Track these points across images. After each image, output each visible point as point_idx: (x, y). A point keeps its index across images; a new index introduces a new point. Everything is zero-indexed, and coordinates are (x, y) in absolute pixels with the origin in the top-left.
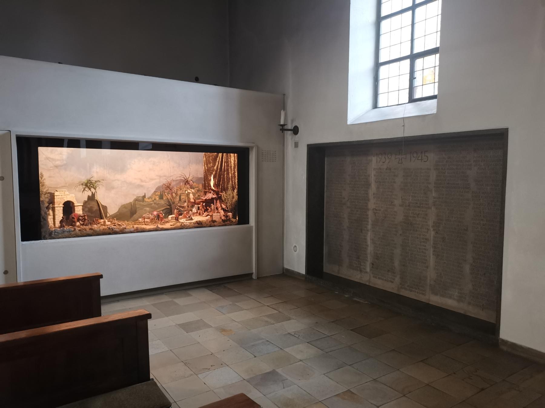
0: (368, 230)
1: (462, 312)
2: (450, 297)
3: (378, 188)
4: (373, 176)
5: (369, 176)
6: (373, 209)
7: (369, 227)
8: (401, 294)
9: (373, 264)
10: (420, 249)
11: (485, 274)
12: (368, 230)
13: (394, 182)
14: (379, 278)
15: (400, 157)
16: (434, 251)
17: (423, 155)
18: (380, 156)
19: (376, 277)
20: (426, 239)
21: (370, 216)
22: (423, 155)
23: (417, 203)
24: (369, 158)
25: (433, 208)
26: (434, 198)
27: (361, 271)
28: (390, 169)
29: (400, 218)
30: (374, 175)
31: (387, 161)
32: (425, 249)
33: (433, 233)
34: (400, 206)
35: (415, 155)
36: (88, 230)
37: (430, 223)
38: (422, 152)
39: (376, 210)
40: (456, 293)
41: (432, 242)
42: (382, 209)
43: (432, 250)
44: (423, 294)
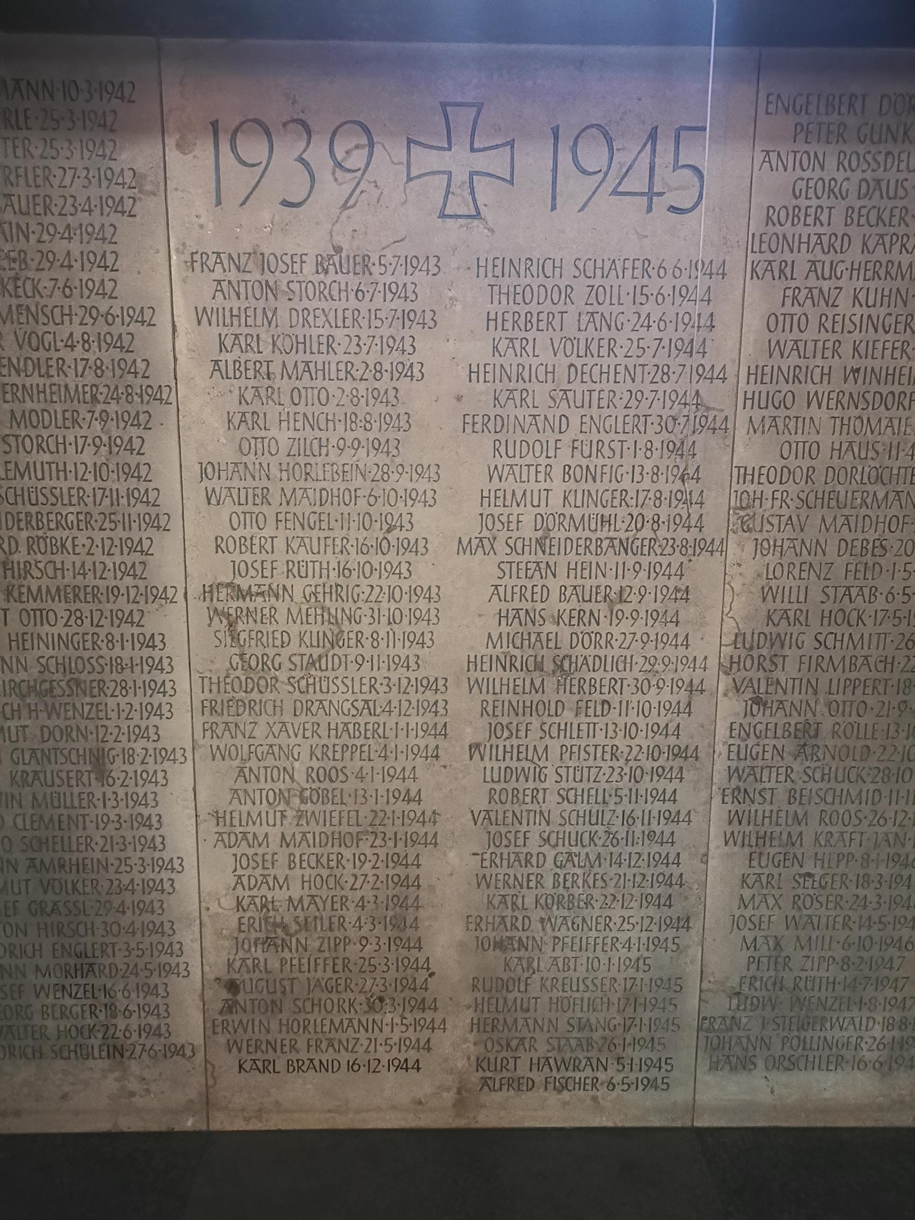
0: (167, 755)
2: (836, 1059)
3: (245, 420)
4: (184, 321)
5: (143, 317)
6: (209, 592)
7: (180, 727)
9: (232, 986)
10: (628, 819)
12: (167, 755)
13: (406, 372)
14: (295, 1067)
15: (459, 161)
16: (735, 818)
17: (665, 156)
18: (253, 148)
19: (267, 1067)
20: (679, 753)
21: (176, 647)
22: (665, 156)
23: (604, 521)
24: (137, 156)
25: (738, 549)
26: (744, 474)
27: (117, 1052)
28: (363, 264)
29: (465, 621)
30: (201, 316)
31: (331, 190)
32: (672, 818)
33: (729, 709)
34: (689, 947)
35: (594, 155)
36: (831, 162)
37: (711, 643)
38: (653, 136)
39: (241, 594)
40: (877, 1032)
42: (299, 586)
43: (718, 811)
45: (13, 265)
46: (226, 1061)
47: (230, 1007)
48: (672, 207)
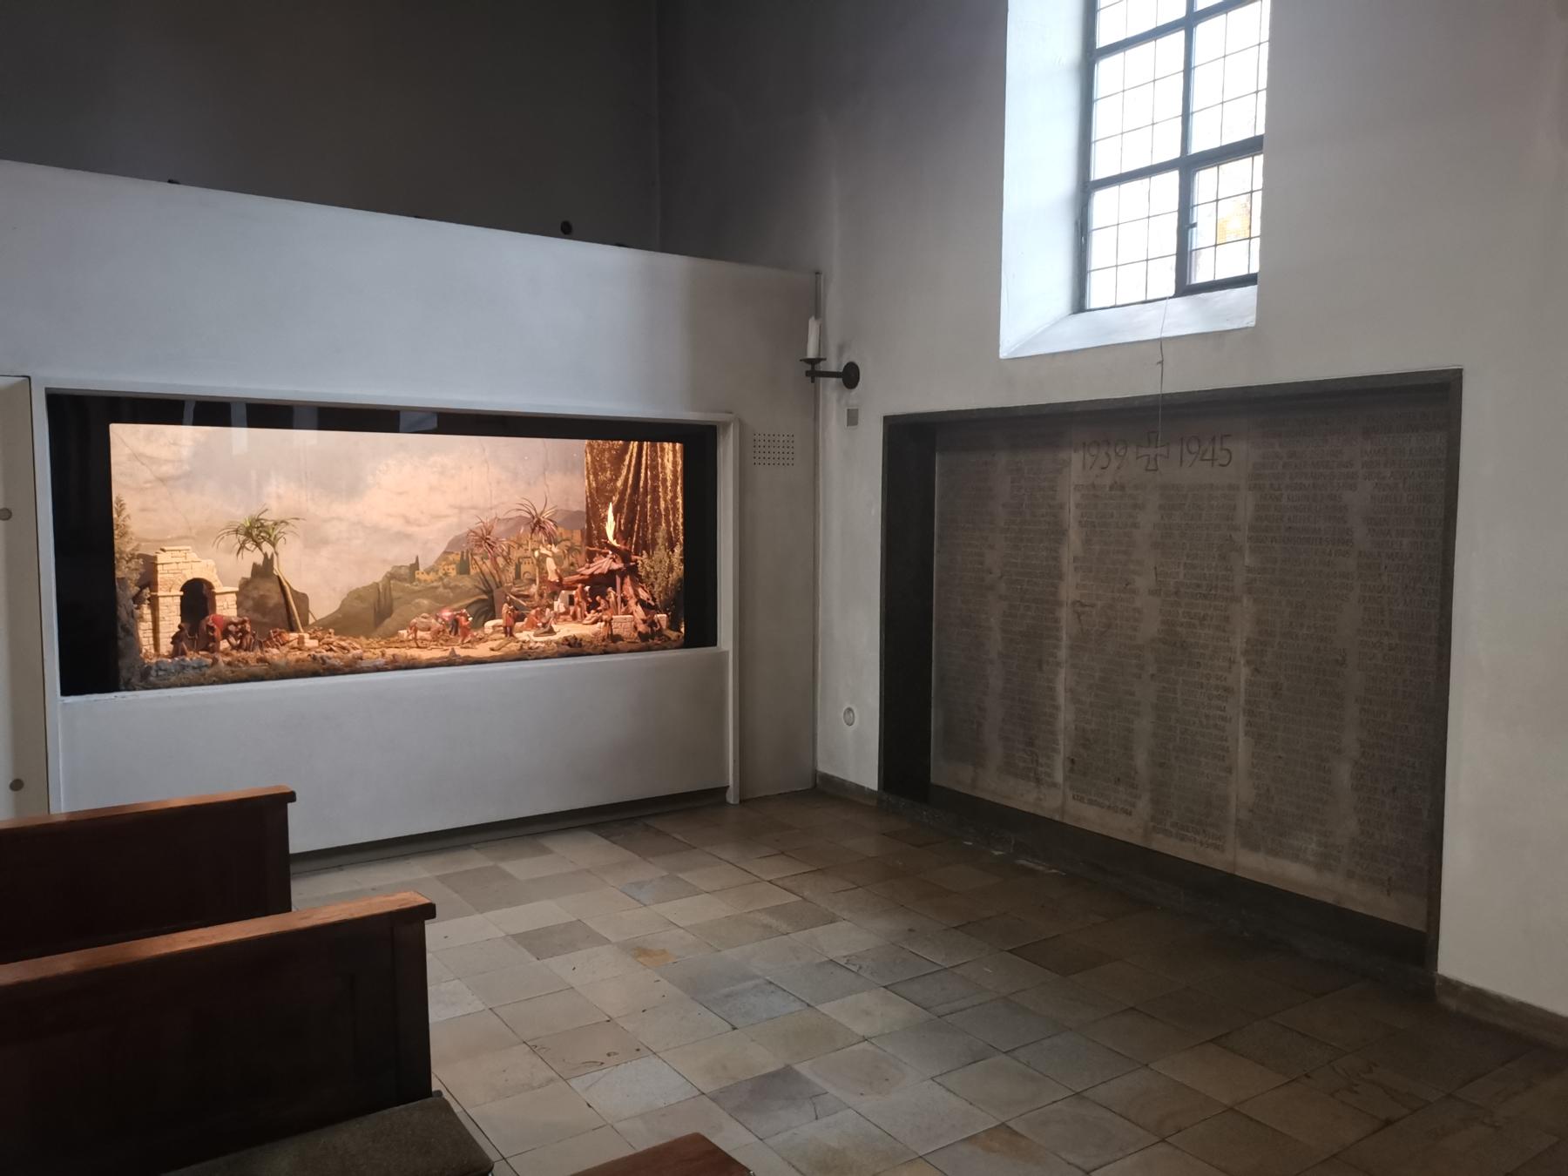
0: (1058, 664)
1: (1330, 900)
2: (1296, 857)
3: (1087, 542)
4: (1073, 508)
5: (1061, 507)
6: (1074, 603)
7: (1063, 654)
8: (1155, 846)
9: (1073, 761)
10: (1207, 716)
11: (1394, 790)
12: (1058, 664)
13: (1135, 525)
14: (1091, 802)
15: (1151, 451)
16: (1249, 724)
17: (1218, 447)
18: (1094, 451)
19: (1081, 800)
20: (1226, 689)
21: (1063, 623)
22: (1218, 447)
23: (1199, 586)
24: (1063, 455)
25: (1246, 601)
26: (1249, 570)
27: (1038, 781)
28: (1122, 488)
29: (1151, 628)
30: (1077, 506)
31: (1115, 464)
32: (1224, 719)
33: (1244, 672)
35: (1194, 447)
37: (1238, 643)
38: (1214, 439)
39: (1083, 605)
40: (1313, 846)
41: (1242, 699)
42: (1099, 603)
43: (1242, 720)
44: (1217, 847)
45: (227, 659)
46: (1070, 794)
47: (1072, 770)
48: (849, 423)
